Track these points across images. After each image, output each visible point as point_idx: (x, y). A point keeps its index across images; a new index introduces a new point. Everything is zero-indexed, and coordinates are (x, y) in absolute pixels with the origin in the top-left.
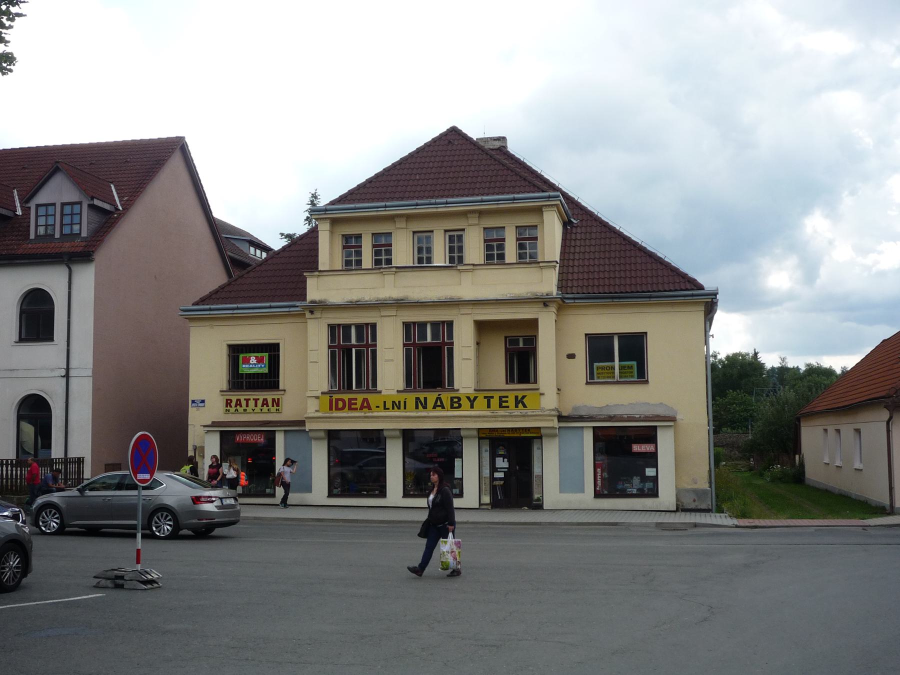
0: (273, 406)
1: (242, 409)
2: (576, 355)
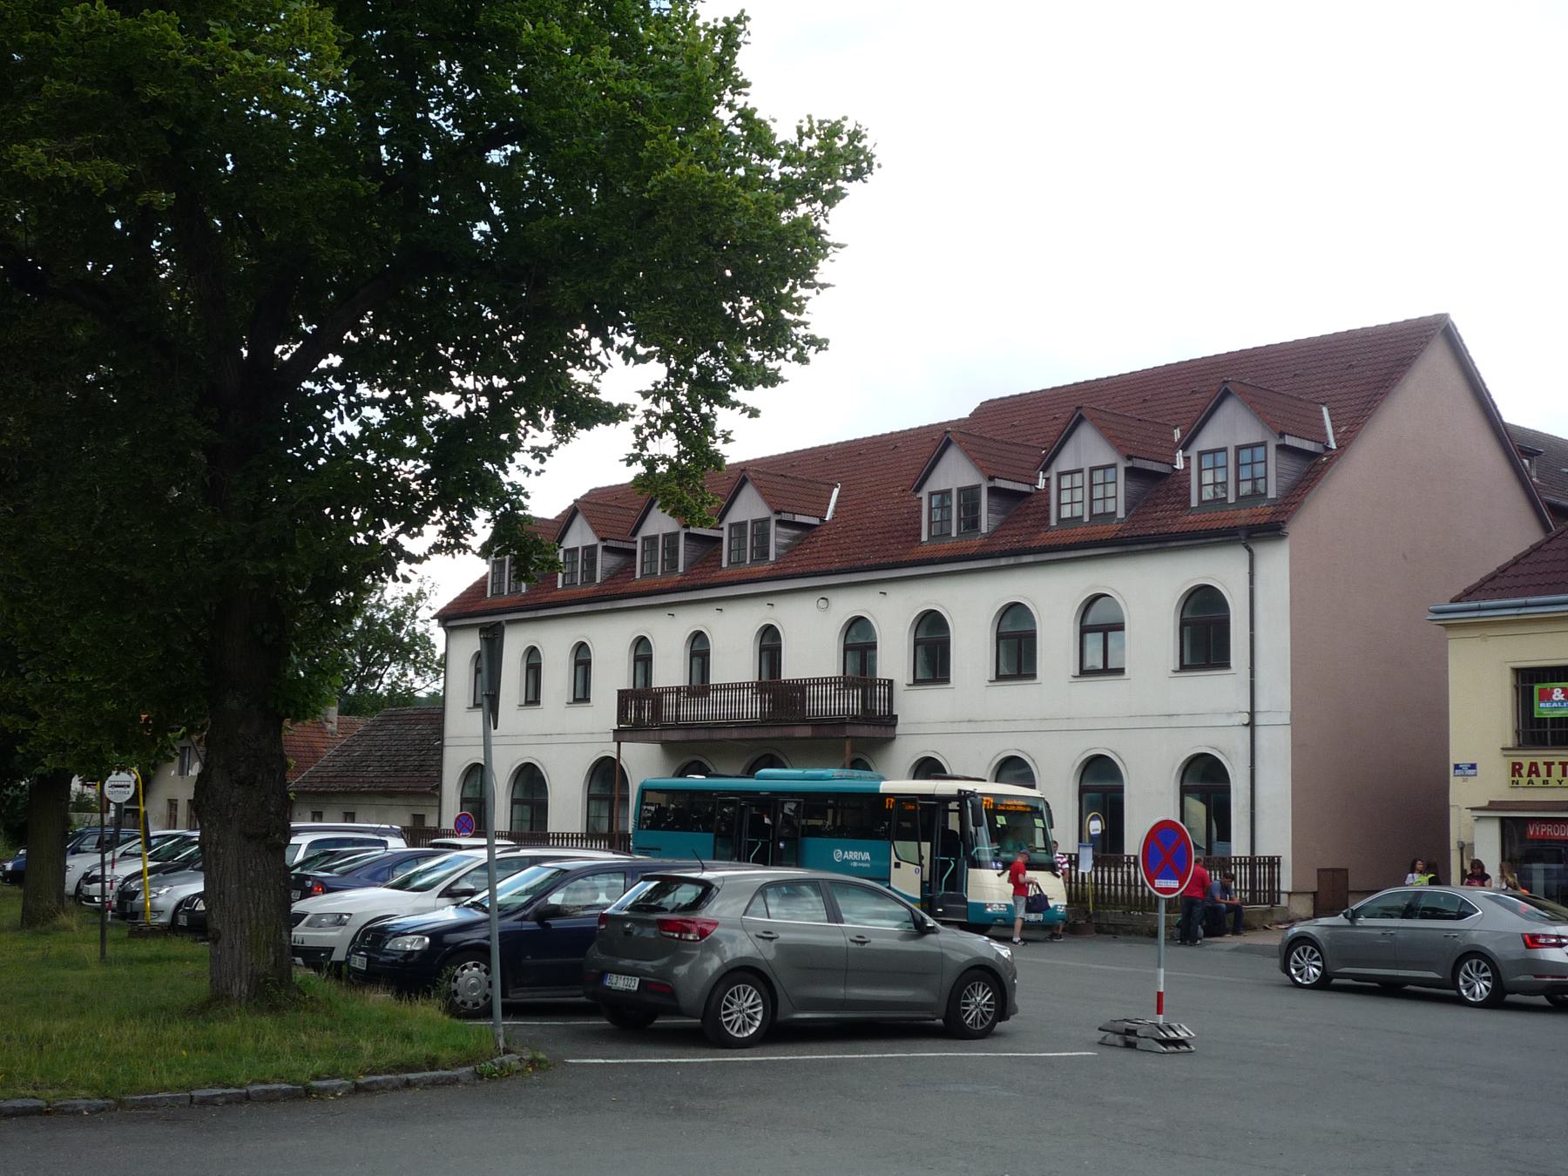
1: (1541, 779)
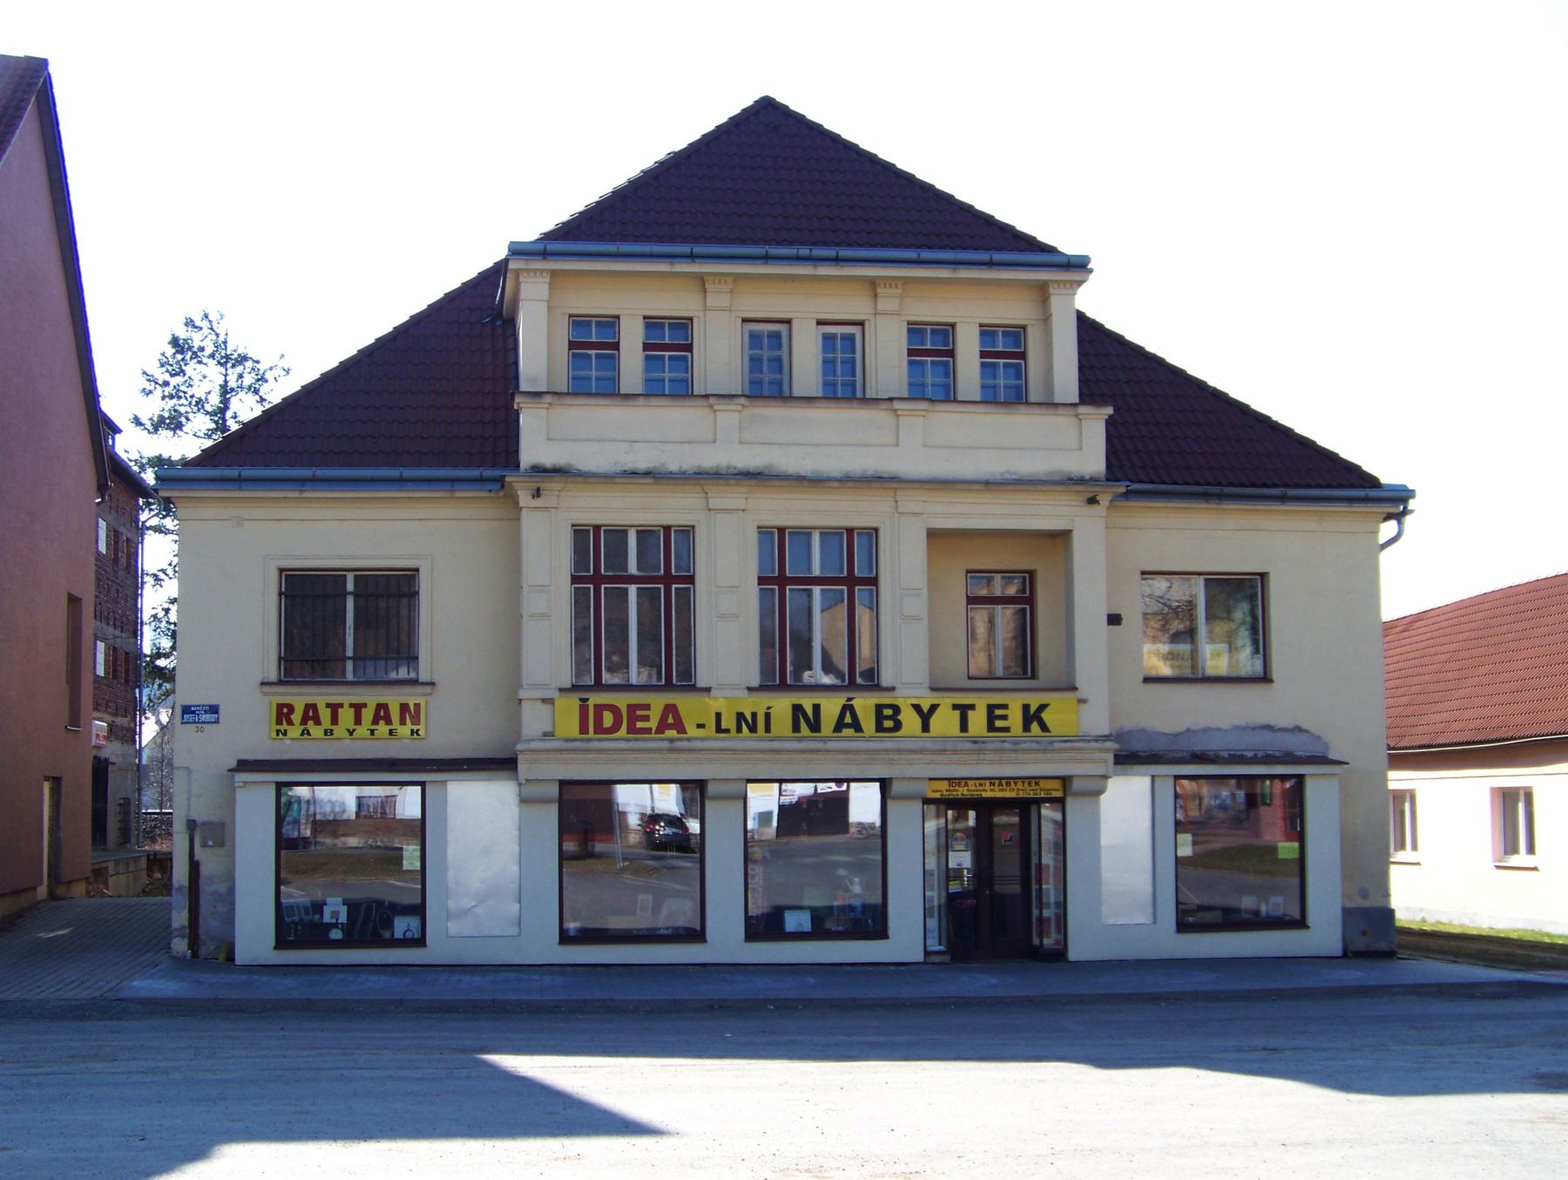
0: (403, 722)
2: (1123, 617)
